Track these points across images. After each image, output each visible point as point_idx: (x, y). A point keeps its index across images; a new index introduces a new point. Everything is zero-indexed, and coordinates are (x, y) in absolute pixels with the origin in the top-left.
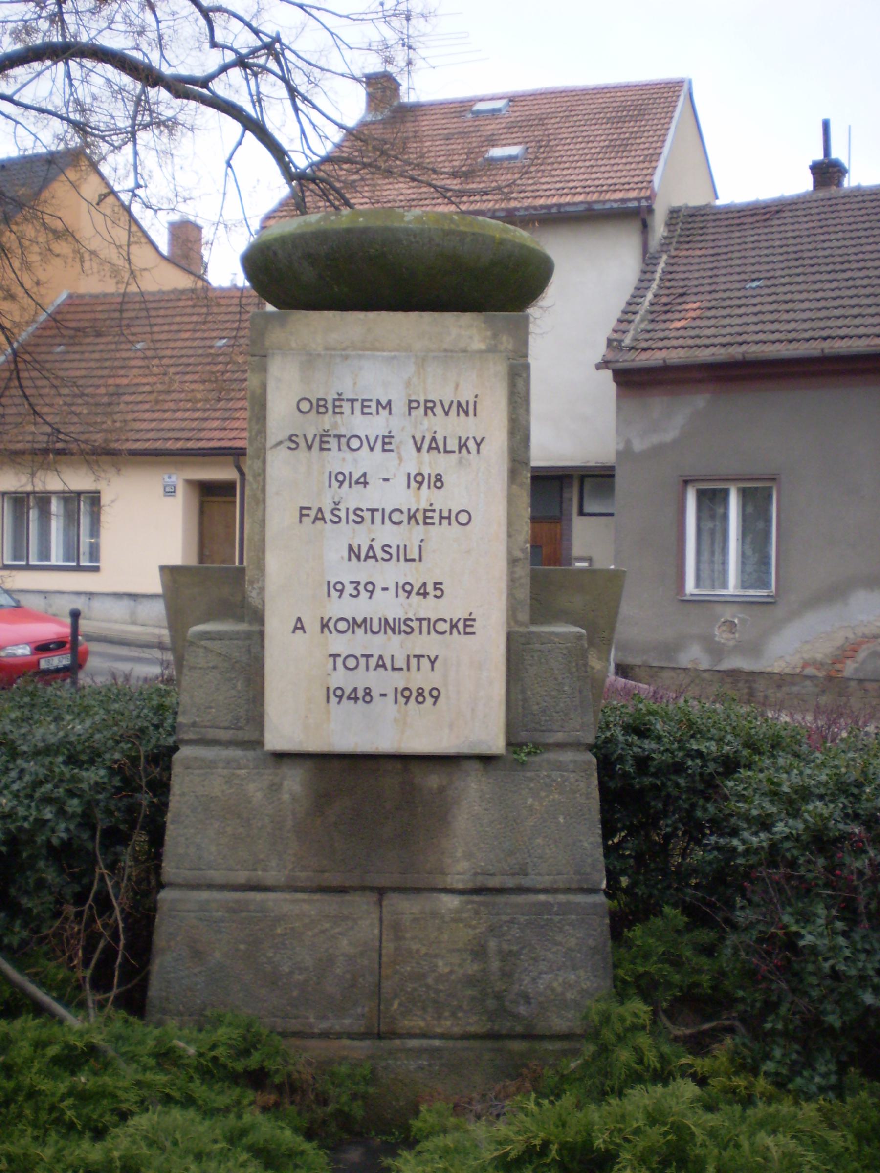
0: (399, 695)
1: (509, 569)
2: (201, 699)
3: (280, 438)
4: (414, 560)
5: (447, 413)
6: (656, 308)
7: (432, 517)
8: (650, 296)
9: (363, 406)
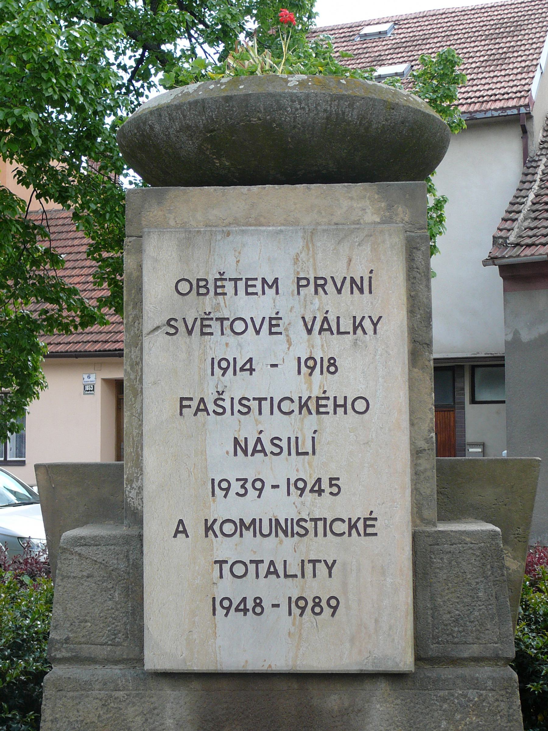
0: (293, 605)
1: (412, 461)
2: (75, 609)
3: (157, 323)
4: (307, 453)
5: (339, 291)
6: (540, 207)
7: (326, 406)
8: (532, 196)
9: (247, 286)
